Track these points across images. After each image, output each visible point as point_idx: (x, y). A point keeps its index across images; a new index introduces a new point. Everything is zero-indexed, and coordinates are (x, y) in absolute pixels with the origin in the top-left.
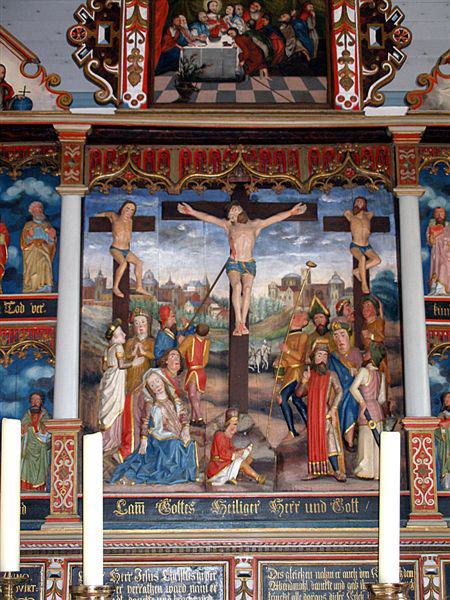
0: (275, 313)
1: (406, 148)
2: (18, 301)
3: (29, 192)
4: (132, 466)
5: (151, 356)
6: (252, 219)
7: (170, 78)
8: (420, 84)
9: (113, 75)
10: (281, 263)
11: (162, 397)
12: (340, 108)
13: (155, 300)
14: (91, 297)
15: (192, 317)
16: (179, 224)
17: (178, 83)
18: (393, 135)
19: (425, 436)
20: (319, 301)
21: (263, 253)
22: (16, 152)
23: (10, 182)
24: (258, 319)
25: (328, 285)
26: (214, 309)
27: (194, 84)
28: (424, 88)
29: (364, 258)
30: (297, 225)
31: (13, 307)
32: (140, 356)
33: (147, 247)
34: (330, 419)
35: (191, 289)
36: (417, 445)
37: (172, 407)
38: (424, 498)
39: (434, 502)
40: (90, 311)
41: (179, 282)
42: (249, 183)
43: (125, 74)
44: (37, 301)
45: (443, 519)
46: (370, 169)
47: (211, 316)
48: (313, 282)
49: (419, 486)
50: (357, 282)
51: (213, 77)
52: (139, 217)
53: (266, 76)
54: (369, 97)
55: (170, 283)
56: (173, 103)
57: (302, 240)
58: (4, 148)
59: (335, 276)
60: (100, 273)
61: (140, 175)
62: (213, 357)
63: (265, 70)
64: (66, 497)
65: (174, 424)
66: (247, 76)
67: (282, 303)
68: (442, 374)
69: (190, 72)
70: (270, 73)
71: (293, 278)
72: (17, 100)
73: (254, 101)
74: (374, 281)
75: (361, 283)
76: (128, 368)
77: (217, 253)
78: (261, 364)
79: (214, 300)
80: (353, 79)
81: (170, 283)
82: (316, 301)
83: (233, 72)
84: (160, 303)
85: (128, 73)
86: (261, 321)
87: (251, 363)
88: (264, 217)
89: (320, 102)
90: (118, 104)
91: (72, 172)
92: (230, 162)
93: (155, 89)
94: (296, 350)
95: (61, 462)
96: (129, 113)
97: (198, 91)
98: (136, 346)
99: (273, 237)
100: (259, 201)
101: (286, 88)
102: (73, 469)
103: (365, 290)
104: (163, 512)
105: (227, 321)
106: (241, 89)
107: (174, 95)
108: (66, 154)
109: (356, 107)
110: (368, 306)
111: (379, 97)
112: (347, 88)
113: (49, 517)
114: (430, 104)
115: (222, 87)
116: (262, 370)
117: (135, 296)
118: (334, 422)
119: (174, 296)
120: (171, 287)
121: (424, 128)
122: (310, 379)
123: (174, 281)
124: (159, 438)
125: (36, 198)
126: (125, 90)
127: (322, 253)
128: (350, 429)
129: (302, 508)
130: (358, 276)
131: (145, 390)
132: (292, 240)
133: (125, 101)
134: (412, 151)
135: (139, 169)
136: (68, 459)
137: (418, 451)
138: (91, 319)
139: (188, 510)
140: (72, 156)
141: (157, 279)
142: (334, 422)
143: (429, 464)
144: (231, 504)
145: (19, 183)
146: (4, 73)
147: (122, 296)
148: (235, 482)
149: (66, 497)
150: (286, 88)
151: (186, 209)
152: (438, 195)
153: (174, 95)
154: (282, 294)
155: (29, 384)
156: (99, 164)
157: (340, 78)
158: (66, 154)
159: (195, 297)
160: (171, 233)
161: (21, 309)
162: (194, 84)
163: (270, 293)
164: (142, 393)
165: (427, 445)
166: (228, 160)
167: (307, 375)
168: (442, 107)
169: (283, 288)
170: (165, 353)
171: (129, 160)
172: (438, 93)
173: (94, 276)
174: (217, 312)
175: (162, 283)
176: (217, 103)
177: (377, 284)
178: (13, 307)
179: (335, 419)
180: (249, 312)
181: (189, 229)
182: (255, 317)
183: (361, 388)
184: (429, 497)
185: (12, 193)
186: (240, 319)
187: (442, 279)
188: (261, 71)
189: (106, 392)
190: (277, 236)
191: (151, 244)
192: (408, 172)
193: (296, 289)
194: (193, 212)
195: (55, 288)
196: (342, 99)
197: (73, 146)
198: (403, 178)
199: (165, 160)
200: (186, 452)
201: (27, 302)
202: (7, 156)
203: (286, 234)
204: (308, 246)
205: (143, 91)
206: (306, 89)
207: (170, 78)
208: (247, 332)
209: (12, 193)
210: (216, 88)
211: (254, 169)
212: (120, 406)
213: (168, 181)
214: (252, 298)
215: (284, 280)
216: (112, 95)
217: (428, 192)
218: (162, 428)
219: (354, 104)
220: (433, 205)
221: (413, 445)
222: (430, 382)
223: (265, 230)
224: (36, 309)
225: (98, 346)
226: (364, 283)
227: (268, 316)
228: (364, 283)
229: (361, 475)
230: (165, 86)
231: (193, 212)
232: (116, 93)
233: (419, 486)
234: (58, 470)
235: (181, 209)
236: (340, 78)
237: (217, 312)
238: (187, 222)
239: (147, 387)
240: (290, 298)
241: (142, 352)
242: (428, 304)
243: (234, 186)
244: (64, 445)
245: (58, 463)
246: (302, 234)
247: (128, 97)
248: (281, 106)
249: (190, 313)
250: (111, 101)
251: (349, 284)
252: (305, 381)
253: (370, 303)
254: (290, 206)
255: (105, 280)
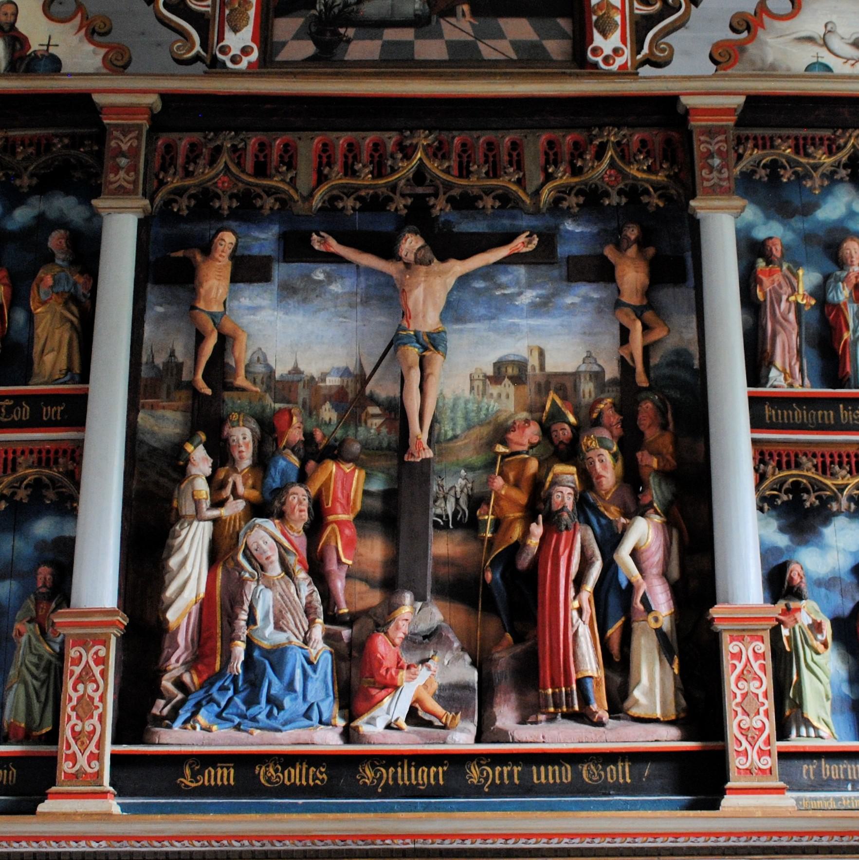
0: (481, 424)
1: (711, 132)
2: (18, 399)
3: (52, 214)
4: (216, 696)
5: (254, 494)
6: (443, 259)
7: (301, 21)
8: (733, 29)
9: (202, 15)
10: (492, 336)
11: (275, 570)
12: (595, 65)
13: (268, 400)
14: (155, 395)
15: (332, 429)
16: (312, 271)
17: (313, 29)
18: (687, 111)
19: (749, 771)
20: (559, 402)
21: (460, 319)
22: (30, 145)
23: (17, 199)
24: (450, 434)
25: (576, 375)
26: (374, 416)
27: (342, 31)
28: (745, 34)
29: (639, 325)
30: (521, 271)
31: (10, 410)
32: (236, 495)
33: (255, 310)
34: (580, 611)
35: (333, 381)
36: (738, 656)
37: (293, 589)
38: (753, 754)
39: (768, 762)
40: (152, 420)
41: (311, 368)
42: (436, 195)
43: (222, 12)
44: (52, 399)
45: (788, 794)
46: (650, 170)
47: (368, 430)
48: (550, 368)
49: (743, 731)
50: (626, 367)
51: (375, 18)
52: (243, 256)
53: (468, 18)
54: (646, 50)
55: (296, 371)
56: (303, 61)
57: (529, 296)
58: (7, 139)
59: (589, 357)
60: (172, 354)
61: (242, 181)
62: (371, 502)
63: (466, 7)
64: (87, 753)
65: (296, 620)
66: (434, 18)
67: (494, 406)
68: (782, 530)
69: (336, 10)
70: (475, 13)
71: (513, 362)
72: (35, 57)
73: (446, 57)
74: (657, 366)
75: (633, 370)
76: (216, 521)
77: (378, 319)
78: (455, 513)
79: (373, 400)
80: (618, 18)
81: (296, 371)
82: (554, 402)
83: (411, 11)
84: (278, 406)
85: (227, 12)
86: (455, 437)
87: (439, 511)
88: (463, 256)
89: (560, 58)
90: (215, 66)
91: (122, 174)
92: (402, 160)
93: (275, 39)
94: (517, 485)
95: (80, 687)
96: (227, 73)
97: (349, 41)
98: (231, 480)
99: (478, 292)
100: (455, 230)
101: (501, 35)
102: (766, 695)
103: (641, 380)
104: (269, 780)
105: (394, 437)
106: (424, 37)
107: (308, 48)
108: (703, 148)
109: (624, 66)
110: (647, 408)
111: (663, 51)
112: (605, 34)
113: (54, 789)
114: (753, 63)
115: (390, 34)
116: (458, 524)
117: (234, 394)
118: (586, 616)
119: (303, 394)
120: (296, 377)
121: (741, 100)
122: (542, 539)
123: (302, 367)
124: (266, 644)
125: (62, 223)
126: (221, 38)
127: (565, 318)
128: (614, 631)
129: (525, 776)
130: (628, 359)
131: (241, 558)
132: (511, 297)
133: (220, 56)
134: (721, 137)
135: (243, 171)
136: (95, 681)
137: (740, 667)
138: (153, 433)
139: (315, 778)
140: (125, 147)
141: (272, 364)
142: (586, 616)
143: (760, 692)
144: (396, 767)
145: (34, 200)
146: (16, 14)
147: (209, 392)
148: (404, 725)
149: (87, 753)
150: (501, 35)
151: (324, 242)
152: (768, 217)
153: (308, 48)
154: (494, 390)
155: (36, 547)
156: (173, 162)
157: (594, 18)
158: (113, 144)
159: (339, 397)
160: (299, 284)
161: (24, 413)
162: (342, 31)
163: (472, 388)
164: (238, 564)
165: (757, 656)
166: (400, 156)
167: (537, 530)
168: (773, 67)
169: (497, 378)
170: (281, 491)
171: (224, 158)
172: (766, 43)
173: (160, 360)
174: (378, 421)
175: (281, 370)
176: (382, 61)
177: (667, 371)
178: (10, 410)
179: (589, 610)
180: (435, 420)
181: (330, 278)
182: (447, 429)
183: (635, 554)
184: (761, 753)
185: (22, 216)
186: (419, 433)
187: (778, 362)
188: (459, 9)
189: (173, 562)
190: (486, 289)
191: (265, 303)
192: (715, 174)
193: (518, 380)
194: (335, 247)
195: (85, 376)
196: (596, 51)
197: (125, 130)
198: (706, 184)
199: (289, 160)
200: (315, 671)
201: (35, 400)
202: (14, 153)
203: (500, 286)
204: (541, 307)
205: (253, 40)
206: (534, 37)
207: (301, 21)
208: (429, 454)
209: (22, 216)
210: (380, 37)
211: (594, 774)
212: (242, 658)
213: (292, 192)
214: (441, 396)
215: (499, 366)
216: (198, 48)
217: (751, 213)
218: (272, 626)
219: (619, 61)
220: (761, 234)
221: (734, 656)
222: (762, 544)
223: (464, 280)
224: (49, 412)
225: (162, 480)
226: (639, 367)
227: (469, 427)
228: (639, 367)
229: (635, 712)
230: (291, 36)
231: (335, 247)
232: (205, 44)
233: (743, 731)
234: (74, 702)
235: (316, 243)
236: (594, 18)
237: (378, 421)
238: (328, 267)
239: (249, 556)
240: (508, 396)
241: (241, 490)
242: (754, 402)
243: (409, 201)
244: (88, 658)
245: (75, 690)
246: (530, 286)
247: (224, 50)
248: (495, 63)
249: (329, 423)
250: (197, 58)
251: (612, 371)
252: (534, 542)
253: (650, 405)
254: (507, 238)
255: (180, 366)
